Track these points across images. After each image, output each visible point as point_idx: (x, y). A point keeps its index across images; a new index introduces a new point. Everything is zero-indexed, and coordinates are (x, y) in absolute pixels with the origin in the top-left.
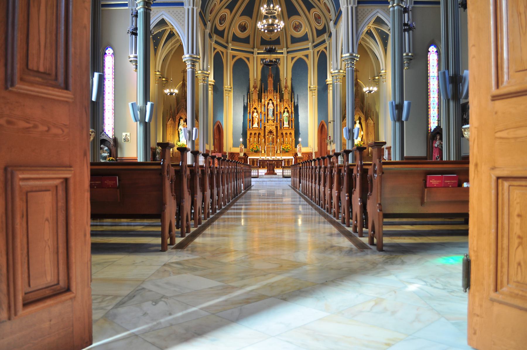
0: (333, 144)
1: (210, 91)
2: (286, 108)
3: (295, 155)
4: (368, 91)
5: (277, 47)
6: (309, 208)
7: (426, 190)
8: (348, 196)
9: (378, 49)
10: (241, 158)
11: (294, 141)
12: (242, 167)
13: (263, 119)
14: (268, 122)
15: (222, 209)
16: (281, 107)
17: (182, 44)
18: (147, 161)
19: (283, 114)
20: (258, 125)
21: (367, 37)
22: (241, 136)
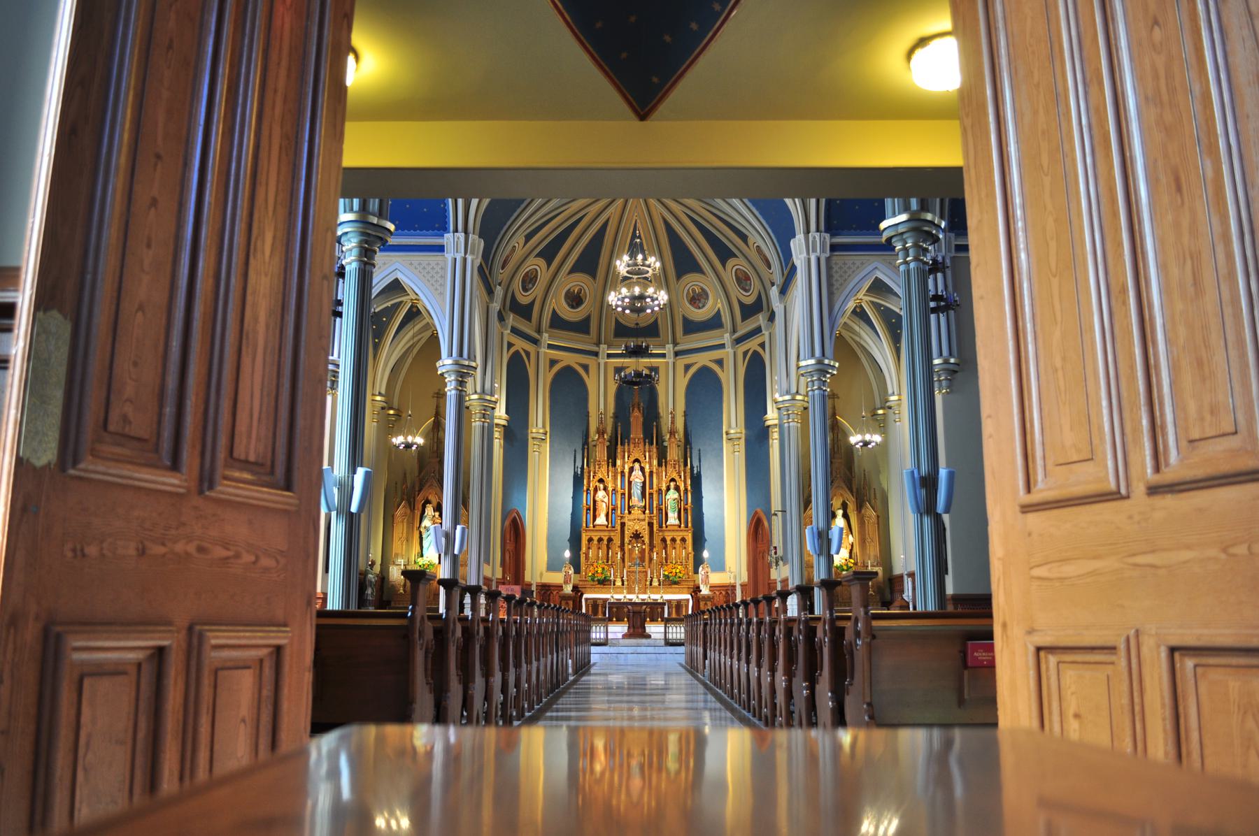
0: (784, 564)
1: (498, 440)
2: (673, 480)
3: (694, 592)
4: (861, 444)
5: (651, 341)
6: (726, 717)
7: (966, 672)
8: (807, 688)
9: (881, 350)
10: (566, 598)
11: (691, 557)
12: (570, 619)
13: (619, 506)
14: (630, 513)
15: (524, 718)
16: (662, 479)
17: (437, 333)
18: (349, 608)
19: (666, 495)
20: (607, 520)
21: (855, 323)
22: (568, 544)
